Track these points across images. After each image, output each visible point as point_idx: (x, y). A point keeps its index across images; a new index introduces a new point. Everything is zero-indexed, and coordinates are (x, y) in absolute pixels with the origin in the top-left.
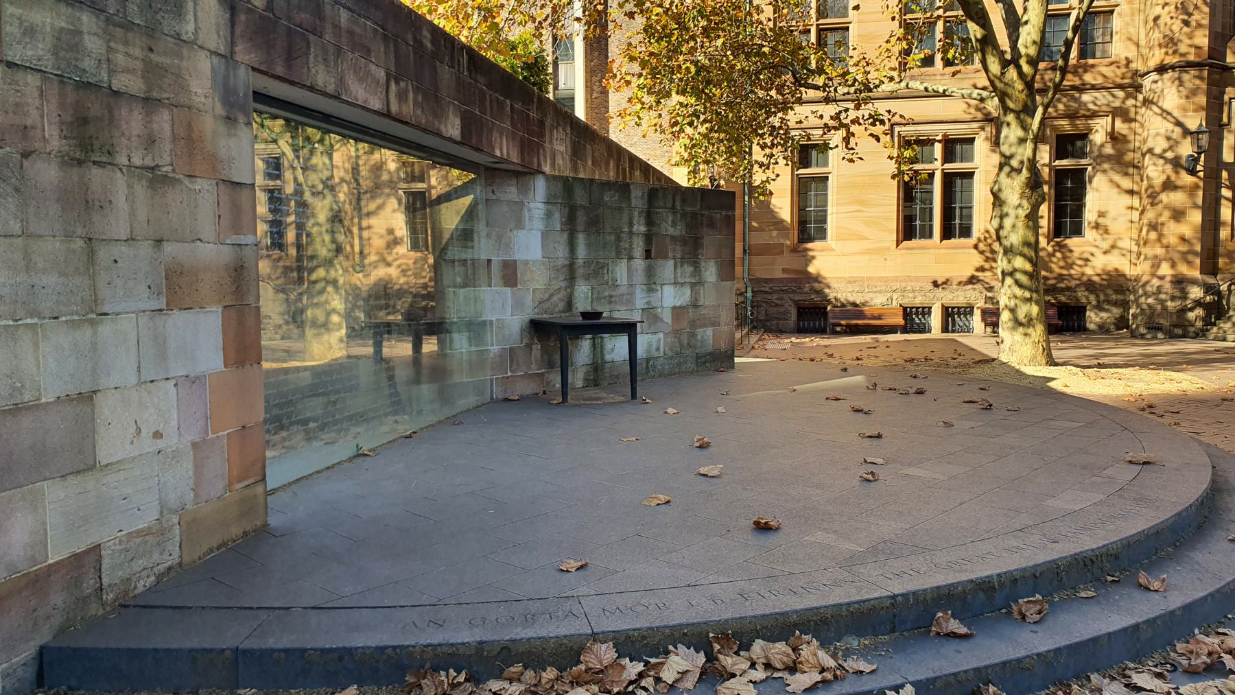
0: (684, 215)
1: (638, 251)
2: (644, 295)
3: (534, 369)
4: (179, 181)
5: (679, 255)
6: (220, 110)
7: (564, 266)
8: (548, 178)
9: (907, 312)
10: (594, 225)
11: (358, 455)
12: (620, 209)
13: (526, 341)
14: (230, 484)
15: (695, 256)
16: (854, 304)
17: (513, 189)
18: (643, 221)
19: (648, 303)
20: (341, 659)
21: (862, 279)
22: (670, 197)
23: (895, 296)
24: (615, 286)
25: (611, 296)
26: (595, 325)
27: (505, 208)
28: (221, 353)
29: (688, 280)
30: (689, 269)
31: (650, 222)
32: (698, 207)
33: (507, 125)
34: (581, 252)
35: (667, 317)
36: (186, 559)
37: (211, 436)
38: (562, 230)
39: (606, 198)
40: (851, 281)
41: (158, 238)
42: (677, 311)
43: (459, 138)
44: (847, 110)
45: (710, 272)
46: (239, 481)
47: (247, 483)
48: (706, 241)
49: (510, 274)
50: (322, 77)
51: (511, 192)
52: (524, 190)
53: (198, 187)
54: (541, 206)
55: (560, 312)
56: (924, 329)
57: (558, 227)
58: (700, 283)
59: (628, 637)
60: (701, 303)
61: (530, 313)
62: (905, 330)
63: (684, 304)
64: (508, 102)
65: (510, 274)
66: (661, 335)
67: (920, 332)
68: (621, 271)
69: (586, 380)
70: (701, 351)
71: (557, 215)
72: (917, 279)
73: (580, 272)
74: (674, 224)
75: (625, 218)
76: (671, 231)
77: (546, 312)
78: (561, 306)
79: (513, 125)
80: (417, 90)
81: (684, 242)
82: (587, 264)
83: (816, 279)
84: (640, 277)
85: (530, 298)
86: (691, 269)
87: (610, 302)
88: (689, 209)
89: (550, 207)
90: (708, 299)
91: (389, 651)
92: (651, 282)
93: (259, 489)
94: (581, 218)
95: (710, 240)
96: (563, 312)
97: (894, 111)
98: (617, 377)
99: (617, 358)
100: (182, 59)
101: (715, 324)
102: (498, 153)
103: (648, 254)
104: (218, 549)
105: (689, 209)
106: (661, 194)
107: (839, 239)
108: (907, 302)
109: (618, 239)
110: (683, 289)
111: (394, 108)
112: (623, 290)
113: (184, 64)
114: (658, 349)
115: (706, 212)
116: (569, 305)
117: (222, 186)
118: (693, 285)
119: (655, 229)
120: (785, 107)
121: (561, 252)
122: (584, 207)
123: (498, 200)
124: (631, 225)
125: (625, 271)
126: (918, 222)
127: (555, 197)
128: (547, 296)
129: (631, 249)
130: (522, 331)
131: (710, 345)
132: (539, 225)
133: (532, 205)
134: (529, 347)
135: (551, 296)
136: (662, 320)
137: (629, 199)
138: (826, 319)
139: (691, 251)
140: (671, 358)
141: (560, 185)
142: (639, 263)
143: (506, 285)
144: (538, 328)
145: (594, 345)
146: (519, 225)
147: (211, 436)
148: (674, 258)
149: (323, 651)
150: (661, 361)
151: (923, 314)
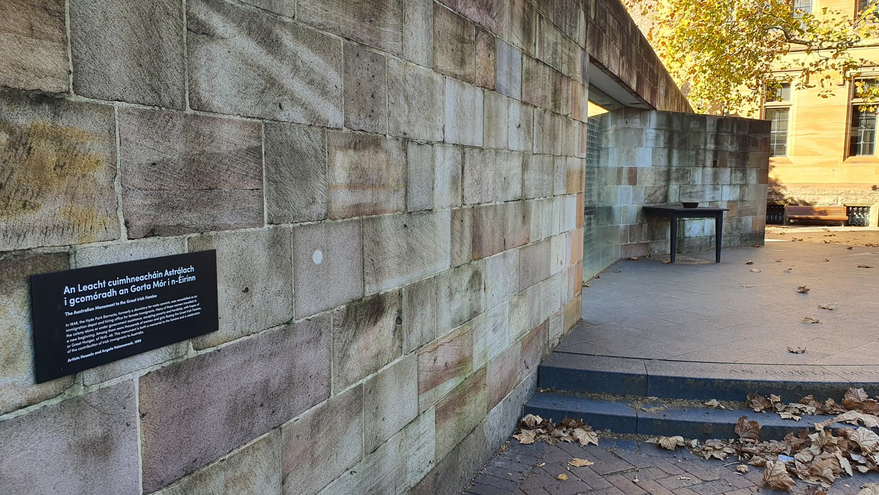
0: (738, 137)
1: (709, 162)
3: (643, 241)
5: (734, 165)
7: (664, 172)
9: (849, 210)
10: (684, 145)
12: (699, 133)
13: (639, 221)
15: (744, 165)
16: (805, 203)
17: (638, 120)
18: (713, 141)
19: (713, 198)
20: (705, 385)
21: (814, 185)
22: (730, 125)
23: (840, 198)
26: (693, 211)
29: (738, 182)
30: (740, 175)
31: (717, 143)
32: (747, 132)
34: (675, 162)
39: (692, 126)
40: (805, 186)
44: (827, 59)
48: (752, 155)
51: (636, 122)
52: (644, 121)
54: (653, 131)
56: (861, 224)
57: (662, 145)
58: (746, 185)
59: (871, 387)
60: (746, 199)
61: (642, 202)
62: (847, 224)
67: (860, 225)
68: (698, 175)
70: (744, 232)
71: (662, 138)
72: (859, 185)
73: (674, 175)
77: (652, 203)
78: (661, 198)
82: (677, 170)
83: (775, 183)
84: (709, 180)
85: (643, 193)
86: (741, 175)
87: (690, 197)
88: (741, 133)
90: (750, 196)
91: (733, 383)
92: (716, 185)
94: (676, 140)
95: (754, 155)
96: (663, 202)
97: (866, 59)
98: (692, 248)
99: (692, 235)
101: (754, 214)
103: (715, 164)
105: (741, 133)
107: (797, 154)
108: (851, 202)
109: (698, 154)
112: (698, 188)
115: (752, 135)
116: (666, 197)
118: (741, 186)
119: (720, 147)
120: (771, 56)
121: (663, 162)
122: (678, 132)
123: (629, 128)
124: (705, 144)
125: (701, 176)
126: (862, 142)
127: (661, 125)
129: (705, 160)
130: (638, 214)
132: (651, 144)
134: (641, 225)
135: (656, 191)
137: (705, 126)
138: (783, 214)
142: (709, 170)
143: (630, 183)
144: (649, 214)
146: (640, 144)
149: (696, 380)
151: (863, 212)
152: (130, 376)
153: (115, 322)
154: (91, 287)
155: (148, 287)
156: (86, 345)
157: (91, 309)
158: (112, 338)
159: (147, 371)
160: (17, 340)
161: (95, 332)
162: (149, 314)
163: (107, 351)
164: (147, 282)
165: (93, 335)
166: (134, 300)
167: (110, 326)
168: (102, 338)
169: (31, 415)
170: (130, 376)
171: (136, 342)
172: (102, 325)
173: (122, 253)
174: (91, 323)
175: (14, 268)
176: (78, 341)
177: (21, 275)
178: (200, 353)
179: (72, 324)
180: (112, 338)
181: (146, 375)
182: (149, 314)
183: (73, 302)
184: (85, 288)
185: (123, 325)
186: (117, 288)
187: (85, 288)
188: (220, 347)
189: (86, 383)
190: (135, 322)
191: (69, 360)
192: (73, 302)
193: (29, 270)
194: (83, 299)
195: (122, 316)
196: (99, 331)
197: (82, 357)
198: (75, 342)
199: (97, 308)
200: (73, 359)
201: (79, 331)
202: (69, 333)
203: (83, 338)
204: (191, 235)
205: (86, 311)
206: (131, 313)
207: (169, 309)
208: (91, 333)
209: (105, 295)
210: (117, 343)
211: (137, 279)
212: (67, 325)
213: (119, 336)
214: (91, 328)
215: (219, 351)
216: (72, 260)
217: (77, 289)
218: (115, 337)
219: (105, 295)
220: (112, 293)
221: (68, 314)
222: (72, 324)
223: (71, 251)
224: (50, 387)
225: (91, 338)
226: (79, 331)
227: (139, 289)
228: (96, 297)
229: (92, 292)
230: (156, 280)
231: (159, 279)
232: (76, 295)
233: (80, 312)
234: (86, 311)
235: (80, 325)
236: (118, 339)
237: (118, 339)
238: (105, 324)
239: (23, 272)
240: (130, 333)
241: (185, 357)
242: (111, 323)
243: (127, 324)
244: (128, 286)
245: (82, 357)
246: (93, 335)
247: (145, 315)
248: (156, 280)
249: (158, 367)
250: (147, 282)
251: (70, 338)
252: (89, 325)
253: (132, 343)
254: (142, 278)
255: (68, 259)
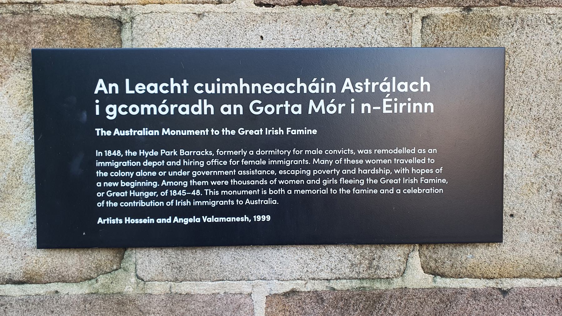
152: (245, 287)
153: (206, 168)
154: (154, 88)
155: (297, 109)
156: (137, 199)
157: (152, 133)
158: (197, 198)
159: (288, 287)
160: (11, 163)
161: (158, 179)
162: (293, 167)
163: (186, 221)
164: (293, 99)
165: (155, 185)
166: (258, 132)
167: (195, 174)
168: (174, 193)
169: (26, 301)
170: (245, 287)
171: (258, 218)
172: (177, 168)
173: (238, 31)
174: (151, 159)
175: (10, 34)
176: (119, 189)
177: (23, 49)
178: (441, 282)
179: (109, 153)
180: (197, 198)
181: (286, 295)
182: (293, 167)
183: (113, 112)
184: (140, 88)
185: (229, 178)
186: (217, 100)
187: (140, 88)
188: (506, 284)
189: (141, 274)
190: (258, 177)
191: (100, 221)
192: (113, 112)
193: (38, 40)
194: (135, 110)
195: (226, 157)
196: (167, 178)
197: (128, 220)
198: (114, 189)
199: (166, 132)
200: (109, 220)
201: (122, 168)
202: (103, 169)
203: (133, 185)
204: (431, 10)
205: (140, 133)
206: (248, 158)
207: (351, 167)
208: (151, 179)
209: (185, 109)
210: (209, 211)
211: (267, 88)
212: (99, 153)
213: (214, 198)
214: (149, 169)
215: (504, 292)
216: (126, 34)
217: (122, 87)
218: (203, 197)
219: (185, 109)
220: (202, 108)
221: (100, 131)
222: (109, 153)
223: (125, 17)
224: (70, 260)
225: (150, 189)
226: (122, 168)
227: (270, 109)
228: (164, 109)
229: (156, 99)
230: (317, 98)
231: (327, 98)
232: (120, 98)
233: (127, 133)
234: (140, 133)
235: (125, 158)
236: (214, 204)
237: (214, 204)
238: (185, 168)
239: (26, 44)
240: (243, 198)
241: (397, 283)
242: (197, 168)
243: (238, 177)
244: (244, 99)
245: (128, 220)
246: (155, 185)
247: (284, 167)
248: (317, 98)
249: (320, 287)
250: (293, 99)
251: (103, 179)
252: (147, 163)
253: (246, 219)
254: (281, 88)
255: (120, 31)
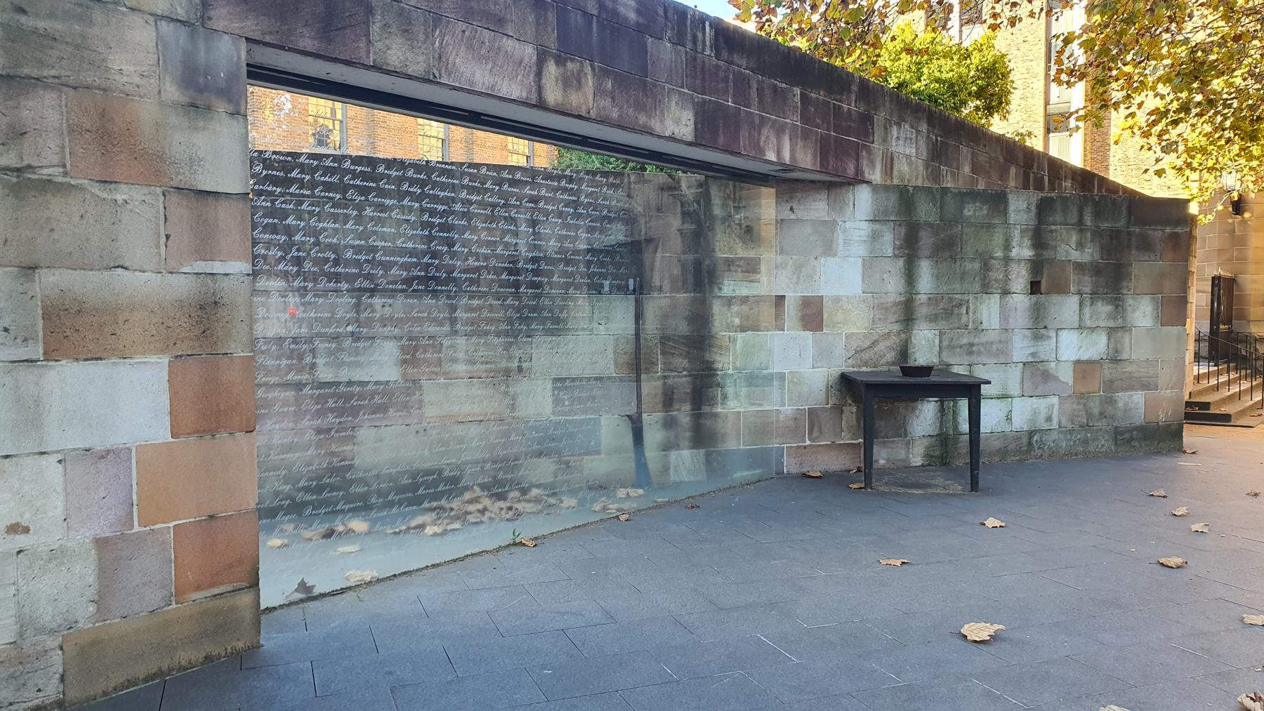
0: (1097, 233)
1: (1020, 278)
2: (1026, 343)
4: (80, 188)
5: (1088, 290)
6: (173, 92)
7: (896, 304)
8: (875, 188)
10: (947, 249)
11: (515, 544)
12: (990, 227)
14: (180, 594)
18: (1027, 242)
19: (1033, 354)
24: (979, 330)
25: (971, 345)
27: (808, 229)
28: (168, 418)
30: (1104, 308)
31: (1039, 239)
33: (794, 120)
35: (1066, 375)
36: (73, 695)
37: (137, 528)
38: (895, 256)
39: (966, 213)
41: (27, 261)
42: (1083, 368)
43: (690, 138)
45: (1142, 313)
46: (198, 588)
47: (216, 591)
49: (813, 315)
50: (396, 53)
51: (817, 208)
52: (837, 206)
53: (120, 198)
54: (864, 225)
55: (888, 364)
57: (890, 252)
60: (1124, 356)
61: (840, 364)
63: (1096, 357)
64: (797, 91)
65: (813, 315)
66: (1055, 400)
68: (989, 311)
69: (927, 456)
70: (1124, 424)
73: (922, 311)
74: (1080, 246)
75: (998, 238)
76: (1076, 256)
77: (866, 365)
79: (805, 119)
80: (602, 74)
81: (1095, 270)
82: (933, 300)
86: (1109, 308)
87: (971, 353)
88: (1106, 225)
89: (877, 226)
92: (1039, 325)
93: (245, 599)
94: (926, 240)
95: (1142, 269)
100: (91, 23)
102: (771, 156)
103: (1034, 287)
104: (146, 680)
105: (1106, 225)
106: (1058, 206)
109: (986, 267)
110: (1094, 336)
111: (553, 95)
112: (992, 336)
113: (96, 31)
114: (1049, 419)
117: (174, 199)
119: (1047, 254)
122: (931, 225)
124: (1007, 247)
128: (868, 343)
129: (1007, 279)
131: (1139, 417)
132: (860, 250)
133: (848, 225)
134: (838, 409)
135: (875, 343)
136: (1056, 379)
137: (1005, 213)
139: (1110, 281)
140: (1071, 432)
141: (894, 198)
142: (1020, 300)
145: (942, 410)
147: (137, 528)
148: (1080, 293)
150: (1054, 435)
